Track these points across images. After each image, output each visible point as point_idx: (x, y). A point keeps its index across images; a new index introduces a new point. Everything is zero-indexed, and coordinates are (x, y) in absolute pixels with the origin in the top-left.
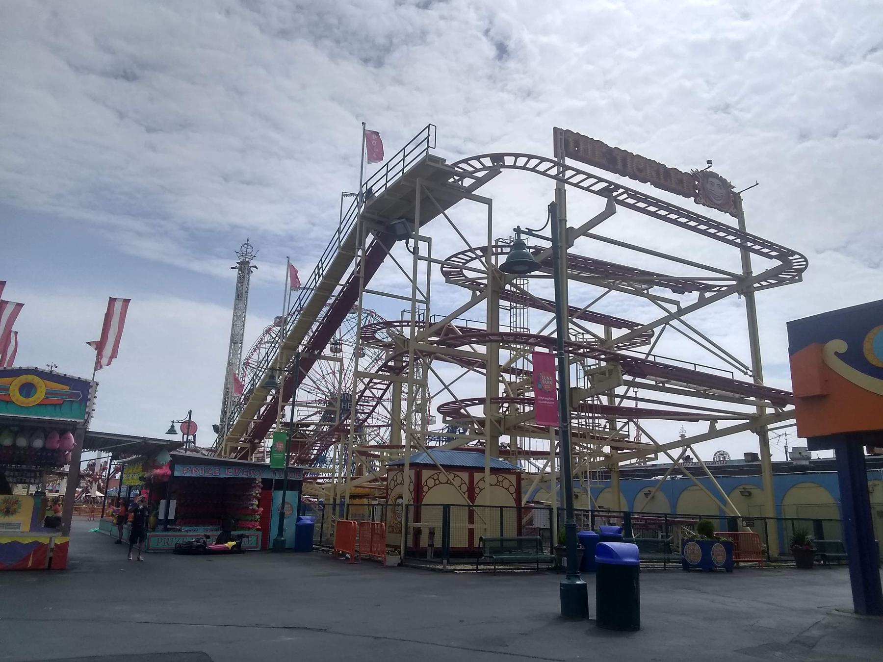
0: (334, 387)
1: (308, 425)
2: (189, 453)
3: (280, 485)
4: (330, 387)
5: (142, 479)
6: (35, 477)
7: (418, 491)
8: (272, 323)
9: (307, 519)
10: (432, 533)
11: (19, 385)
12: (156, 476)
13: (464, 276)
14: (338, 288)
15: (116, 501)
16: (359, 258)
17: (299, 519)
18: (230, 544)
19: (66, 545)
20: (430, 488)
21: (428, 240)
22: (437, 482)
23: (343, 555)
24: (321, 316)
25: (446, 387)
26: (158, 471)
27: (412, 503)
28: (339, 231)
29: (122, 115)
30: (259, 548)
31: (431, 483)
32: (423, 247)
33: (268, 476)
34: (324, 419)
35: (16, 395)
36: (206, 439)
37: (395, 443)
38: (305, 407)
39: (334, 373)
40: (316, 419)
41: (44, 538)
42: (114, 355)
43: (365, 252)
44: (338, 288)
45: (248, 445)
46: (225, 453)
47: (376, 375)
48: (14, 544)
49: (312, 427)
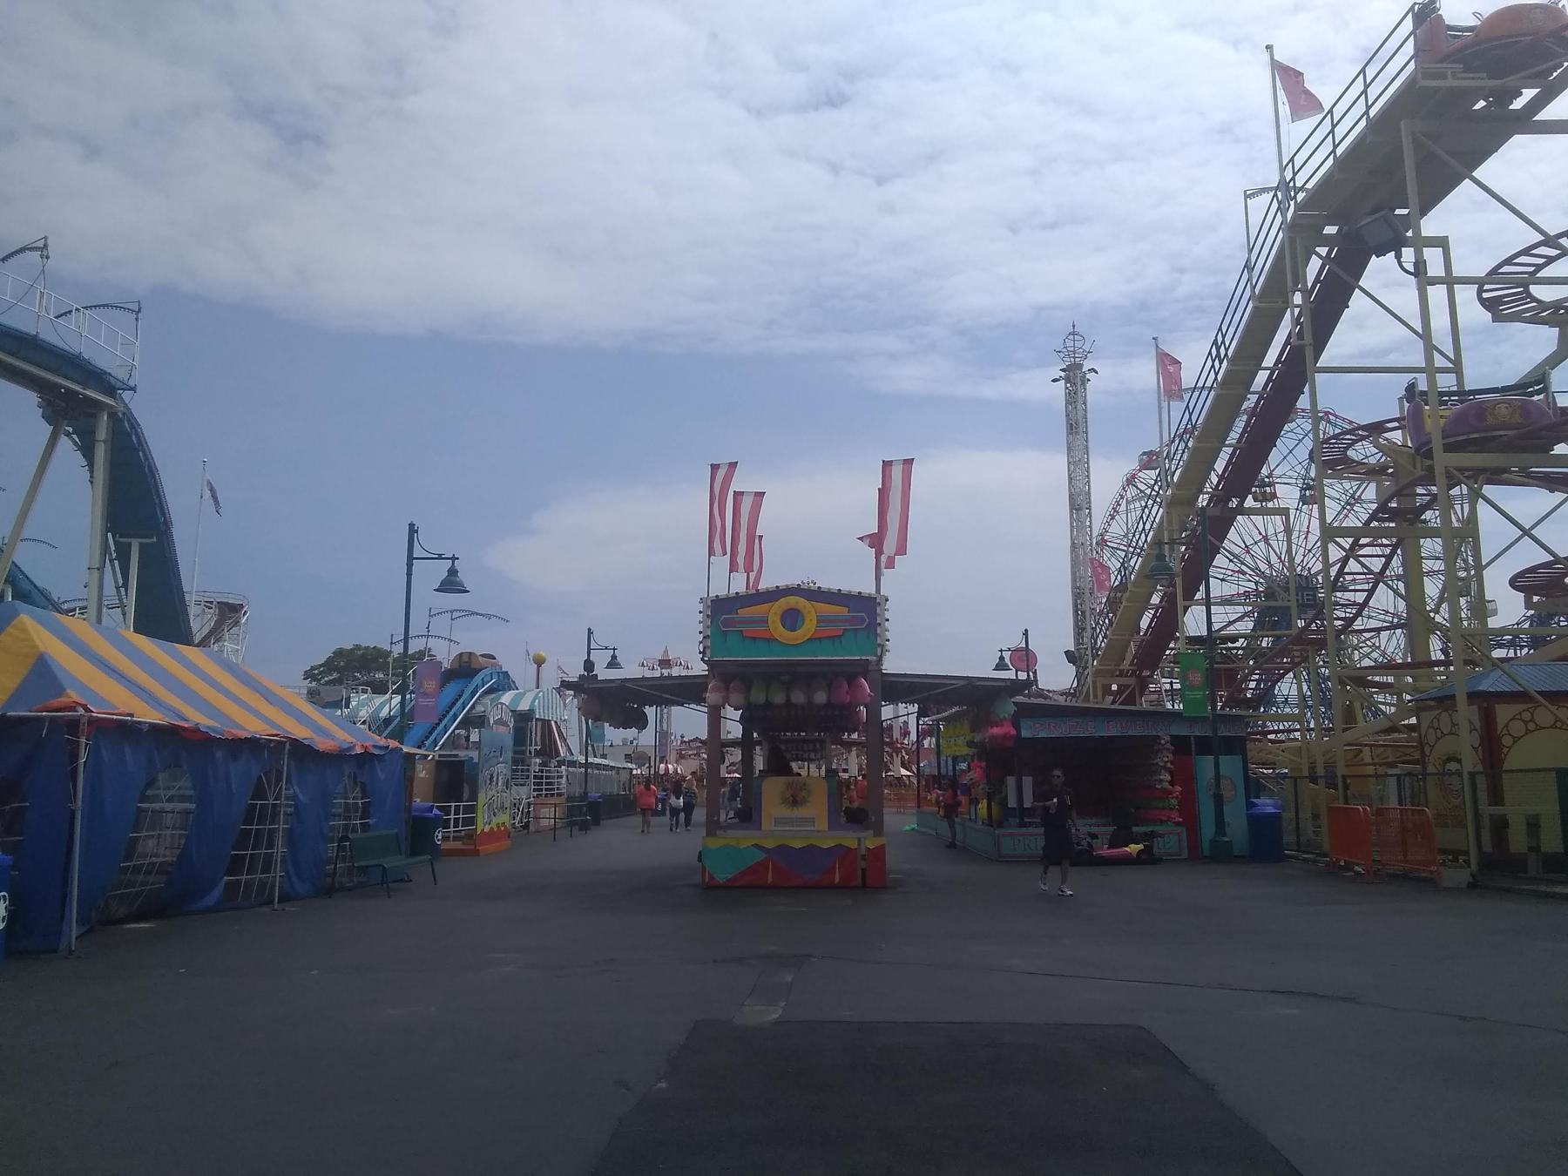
0: (1270, 566)
1: (1234, 639)
2: (1033, 700)
3: (1205, 746)
4: (1263, 567)
5: (971, 744)
6: (815, 750)
7: (1491, 745)
8: (1135, 465)
9: (1266, 805)
10: (1533, 825)
11: (779, 612)
12: (993, 738)
13: (1534, 299)
14: (1262, 377)
15: (935, 780)
16: (1297, 311)
17: (1250, 805)
18: (1134, 848)
19: (881, 849)
20: (1516, 740)
21: (1442, 243)
22: (1531, 726)
23: (1349, 867)
24: (1234, 436)
25: (1526, 533)
26: (995, 731)
27: (1480, 768)
28: (1249, 267)
29: (835, 168)
30: (1185, 855)
31: (1517, 728)
32: (1433, 257)
33: (1181, 730)
34: (1259, 625)
35: (779, 631)
36: (1056, 676)
37: (1419, 659)
38: (1221, 610)
39: (1266, 539)
40: (1247, 626)
41: (849, 839)
42: (902, 549)
43: (1307, 293)
44: (1262, 377)
45: (1132, 681)
46: (1095, 696)
47: (1366, 530)
48: (811, 847)
49: (1241, 642)
